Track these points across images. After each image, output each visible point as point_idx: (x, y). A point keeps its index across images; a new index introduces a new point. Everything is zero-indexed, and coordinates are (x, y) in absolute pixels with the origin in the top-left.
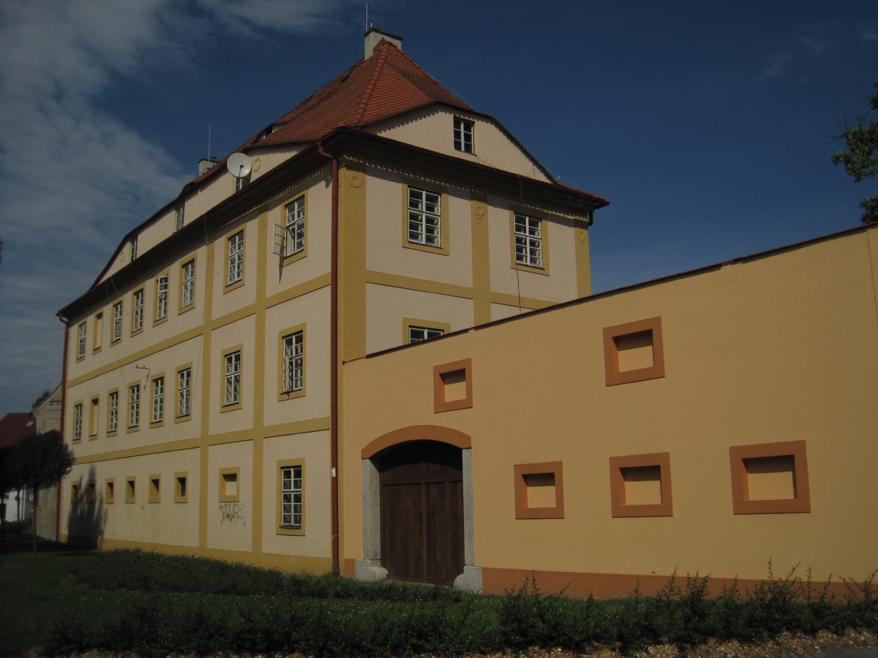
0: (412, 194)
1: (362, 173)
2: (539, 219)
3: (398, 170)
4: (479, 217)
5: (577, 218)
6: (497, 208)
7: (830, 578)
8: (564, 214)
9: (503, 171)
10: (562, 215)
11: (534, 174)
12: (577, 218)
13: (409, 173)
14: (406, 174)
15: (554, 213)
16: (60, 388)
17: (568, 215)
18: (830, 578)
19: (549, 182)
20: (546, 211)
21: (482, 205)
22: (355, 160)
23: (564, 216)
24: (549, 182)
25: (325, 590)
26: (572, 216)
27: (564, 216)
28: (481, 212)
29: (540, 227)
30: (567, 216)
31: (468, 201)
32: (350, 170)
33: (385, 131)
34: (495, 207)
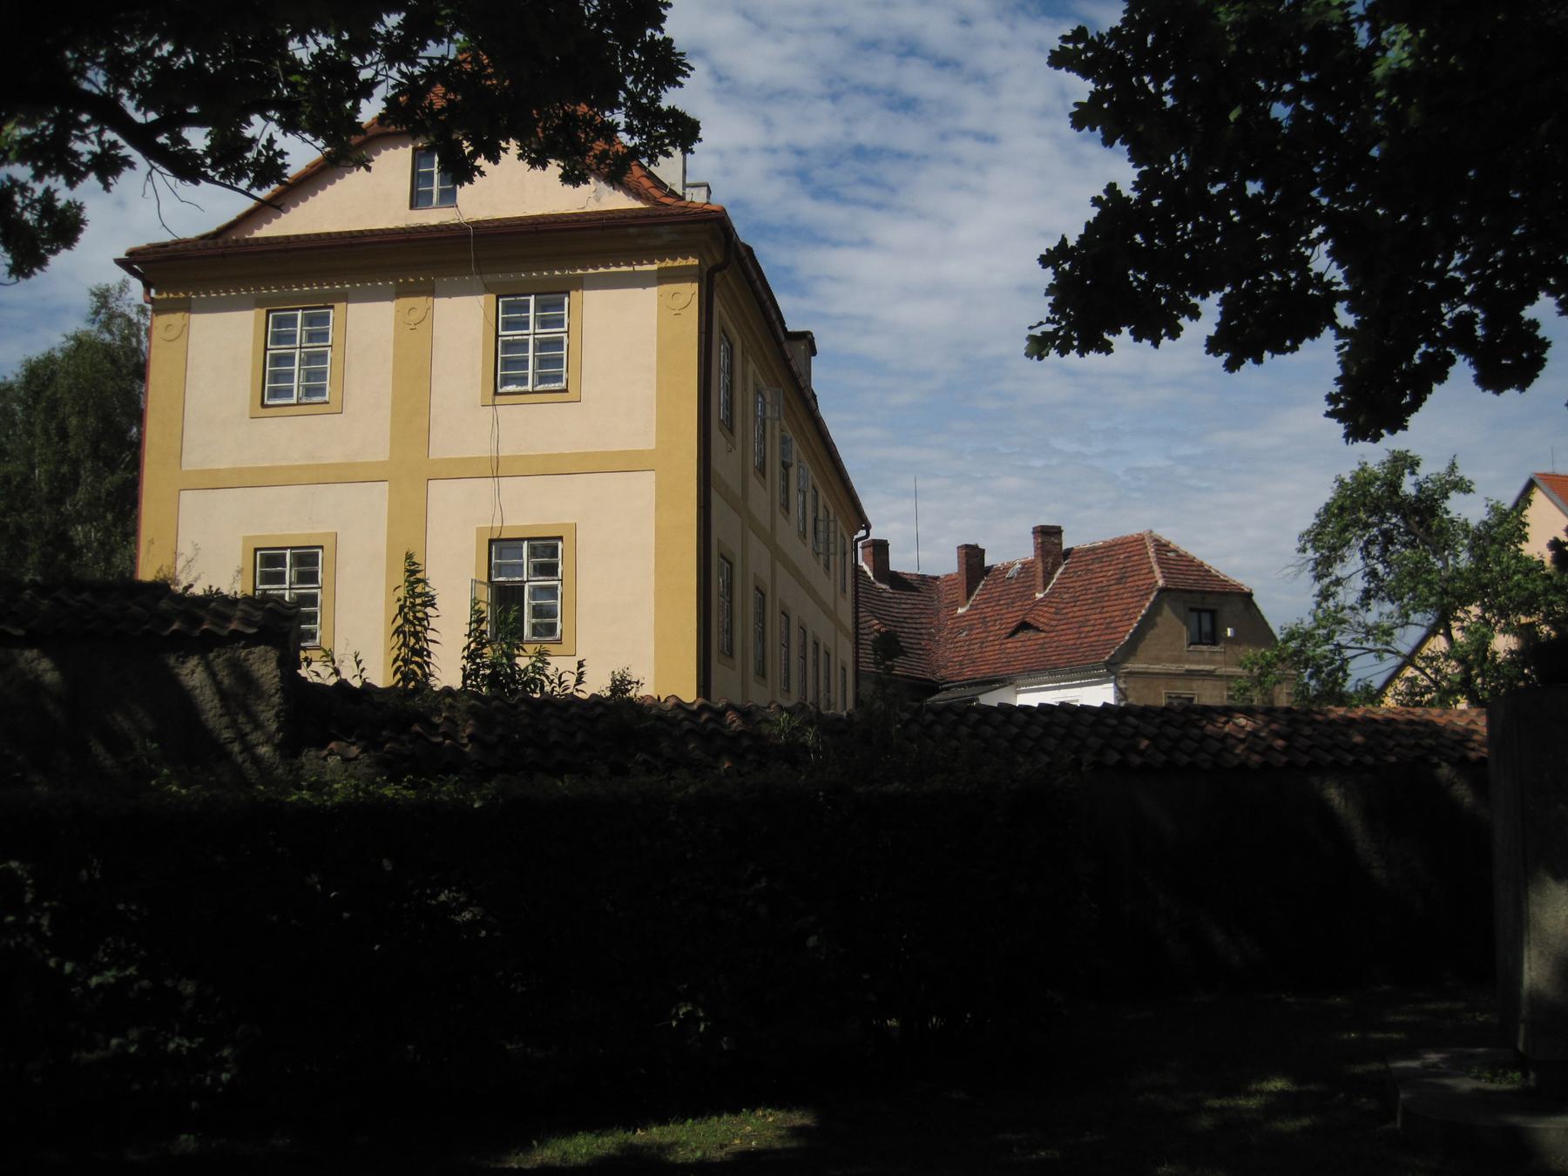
0: (279, 322)
1: (425, 298)
2: (562, 293)
3: (226, 291)
4: (411, 327)
5: (669, 263)
6: (454, 299)
7: (433, 629)
8: (629, 264)
9: (340, 235)
10: (624, 269)
11: (598, 200)
12: (669, 263)
13: (310, 285)
14: (337, 287)
15: (602, 270)
16: (779, 568)
17: (641, 264)
18: (433, 629)
19: (638, 205)
20: (579, 271)
21: (420, 302)
22: (171, 295)
23: (631, 269)
24: (638, 205)
25: (1521, 634)
26: (652, 262)
27: (631, 269)
28: (415, 316)
29: (331, 324)
30: (638, 268)
31: (389, 303)
32: (161, 314)
33: (269, 222)
34: (450, 297)
